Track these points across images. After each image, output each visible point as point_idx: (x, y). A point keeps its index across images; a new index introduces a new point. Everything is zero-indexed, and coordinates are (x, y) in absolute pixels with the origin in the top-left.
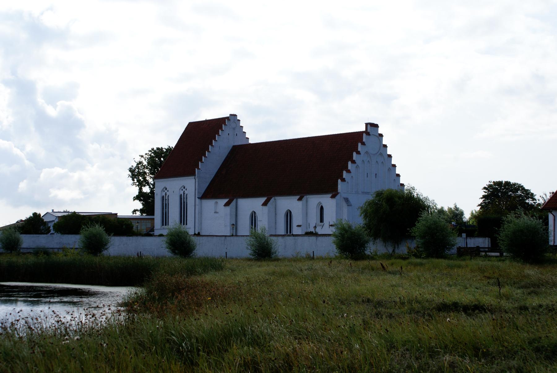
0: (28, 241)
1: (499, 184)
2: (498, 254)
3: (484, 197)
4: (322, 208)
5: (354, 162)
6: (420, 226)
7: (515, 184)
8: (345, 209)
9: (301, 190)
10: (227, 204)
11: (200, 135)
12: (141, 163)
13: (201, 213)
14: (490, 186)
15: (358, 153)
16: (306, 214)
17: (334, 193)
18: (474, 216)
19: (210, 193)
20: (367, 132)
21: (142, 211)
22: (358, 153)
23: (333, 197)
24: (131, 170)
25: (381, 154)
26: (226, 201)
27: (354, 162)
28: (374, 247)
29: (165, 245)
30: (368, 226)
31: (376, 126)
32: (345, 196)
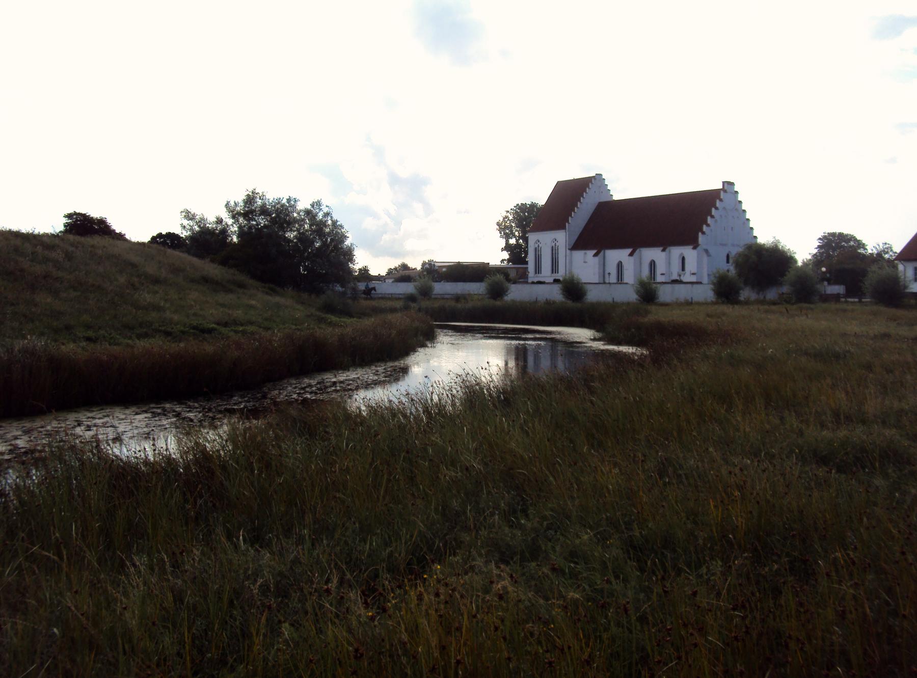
0: (442, 288)
1: (833, 235)
2: (856, 300)
3: (819, 247)
4: (683, 259)
5: (712, 217)
6: (790, 276)
7: (847, 235)
8: (705, 259)
9: (664, 241)
10: (596, 255)
11: (569, 194)
12: (506, 217)
13: (571, 262)
14: (825, 237)
15: (717, 208)
16: (669, 263)
17: (695, 244)
18: (805, 264)
19: (580, 244)
20: (723, 190)
21: (509, 261)
22: (717, 208)
23: (695, 248)
24: (498, 224)
25: (736, 210)
26: (594, 252)
27: (712, 217)
28: (746, 293)
29: (559, 292)
30: (740, 275)
31: (732, 184)
32: (705, 247)
